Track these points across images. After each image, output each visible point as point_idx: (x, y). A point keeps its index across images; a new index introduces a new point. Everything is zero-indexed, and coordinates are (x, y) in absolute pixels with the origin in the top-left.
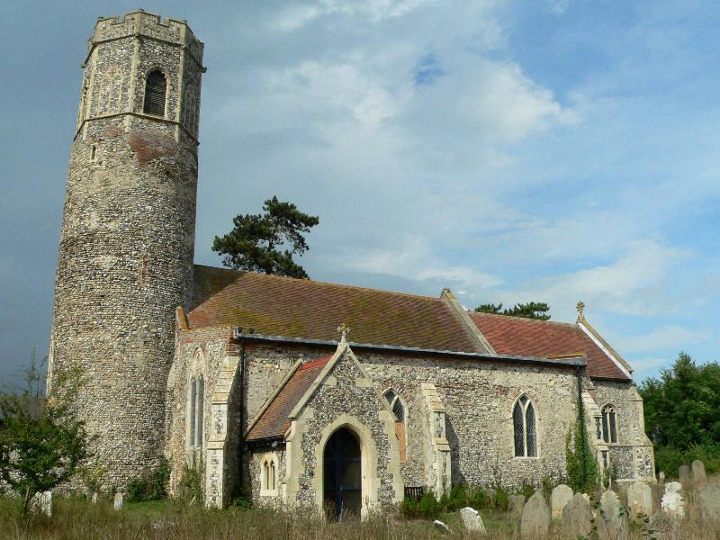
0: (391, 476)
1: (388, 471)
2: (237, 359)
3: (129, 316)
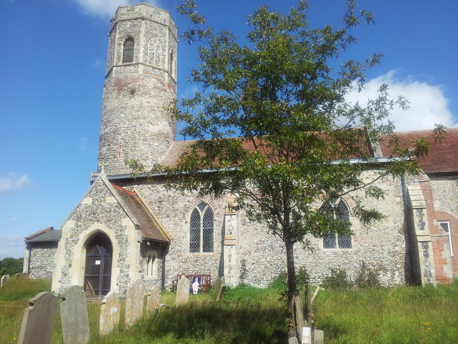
1: (126, 263)
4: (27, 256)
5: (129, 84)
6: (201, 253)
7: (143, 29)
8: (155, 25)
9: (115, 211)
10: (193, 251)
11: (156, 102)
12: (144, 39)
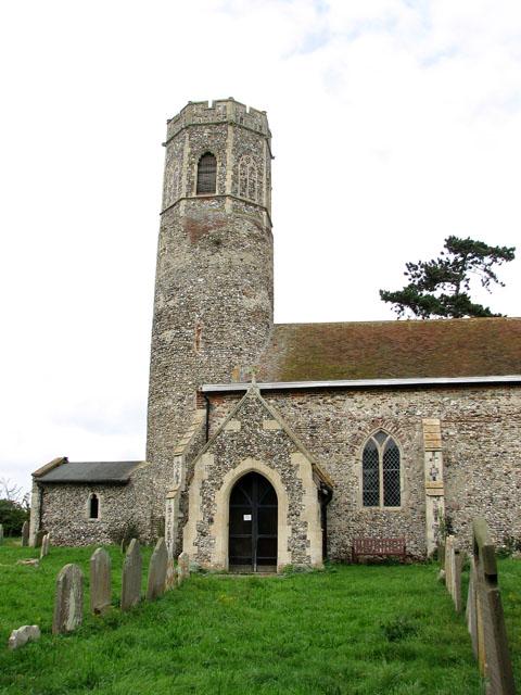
0: (305, 524)
1: (301, 518)
2: (205, 411)
3: (186, 383)
4: (37, 504)
5: (210, 228)
6: (382, 507)
7: (230, 141)
8: (247, 134)
9: (279, 442)
10: (368, 505)
11: (252, 259)
12: (233, 156)
